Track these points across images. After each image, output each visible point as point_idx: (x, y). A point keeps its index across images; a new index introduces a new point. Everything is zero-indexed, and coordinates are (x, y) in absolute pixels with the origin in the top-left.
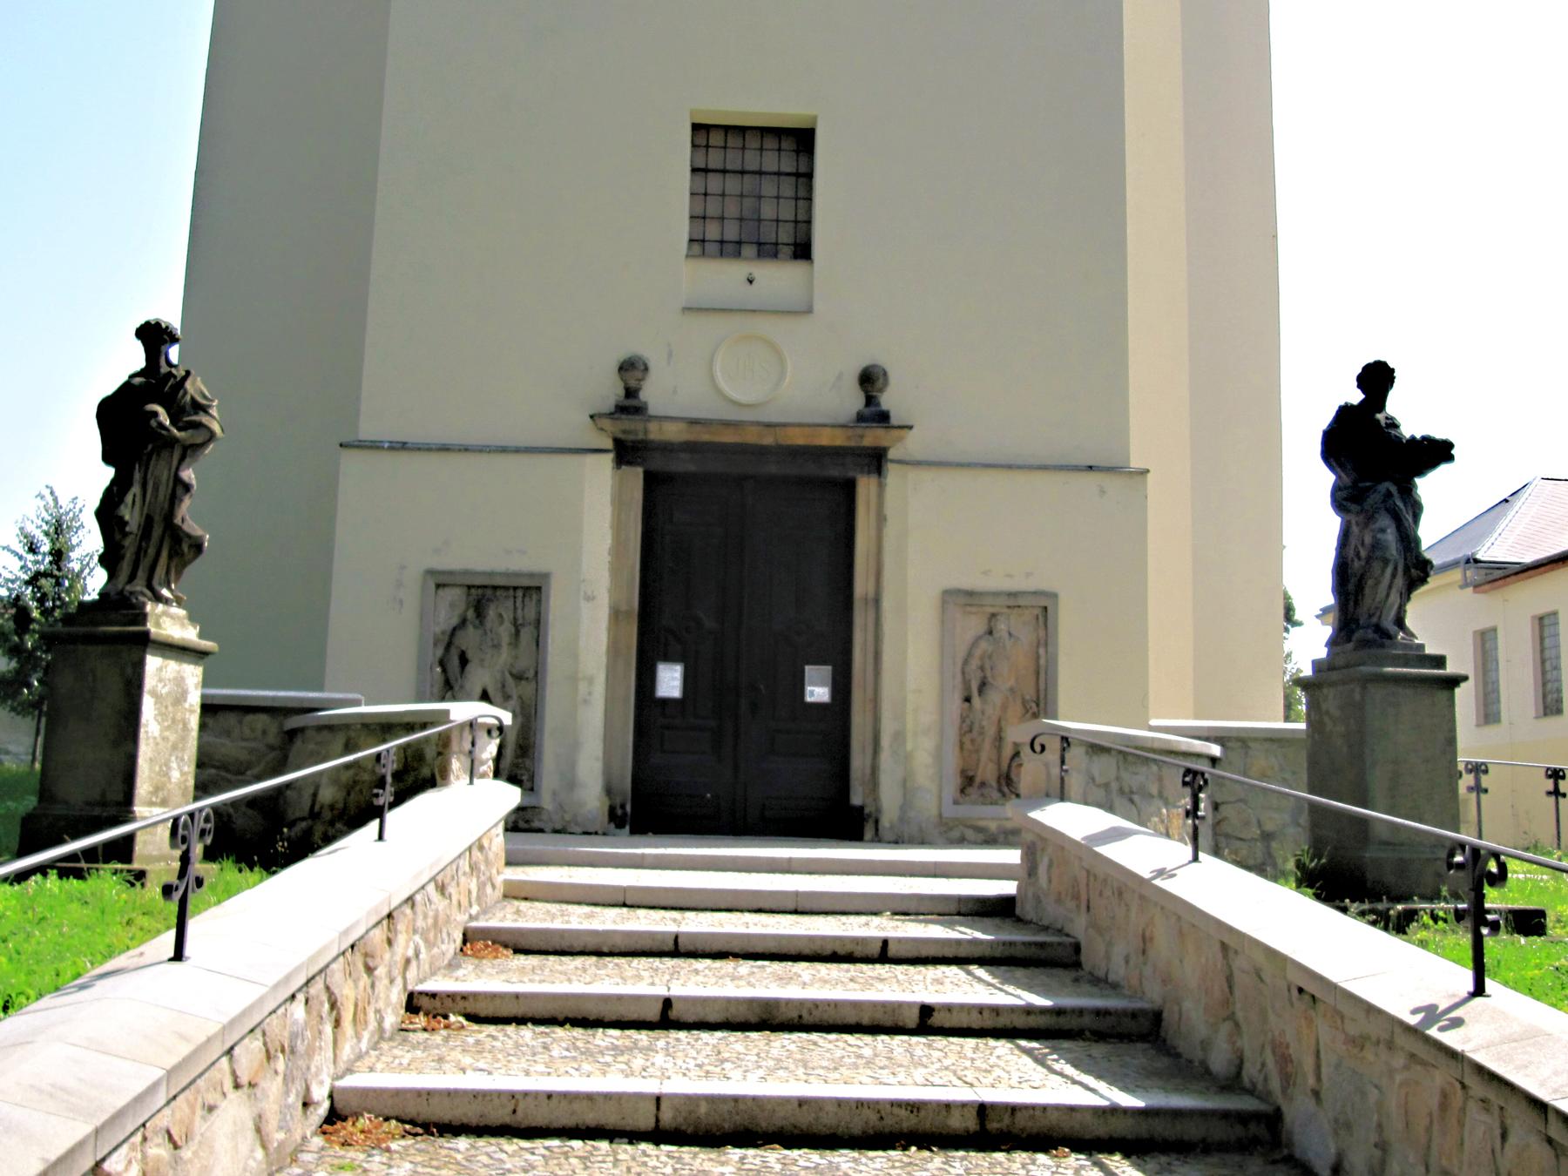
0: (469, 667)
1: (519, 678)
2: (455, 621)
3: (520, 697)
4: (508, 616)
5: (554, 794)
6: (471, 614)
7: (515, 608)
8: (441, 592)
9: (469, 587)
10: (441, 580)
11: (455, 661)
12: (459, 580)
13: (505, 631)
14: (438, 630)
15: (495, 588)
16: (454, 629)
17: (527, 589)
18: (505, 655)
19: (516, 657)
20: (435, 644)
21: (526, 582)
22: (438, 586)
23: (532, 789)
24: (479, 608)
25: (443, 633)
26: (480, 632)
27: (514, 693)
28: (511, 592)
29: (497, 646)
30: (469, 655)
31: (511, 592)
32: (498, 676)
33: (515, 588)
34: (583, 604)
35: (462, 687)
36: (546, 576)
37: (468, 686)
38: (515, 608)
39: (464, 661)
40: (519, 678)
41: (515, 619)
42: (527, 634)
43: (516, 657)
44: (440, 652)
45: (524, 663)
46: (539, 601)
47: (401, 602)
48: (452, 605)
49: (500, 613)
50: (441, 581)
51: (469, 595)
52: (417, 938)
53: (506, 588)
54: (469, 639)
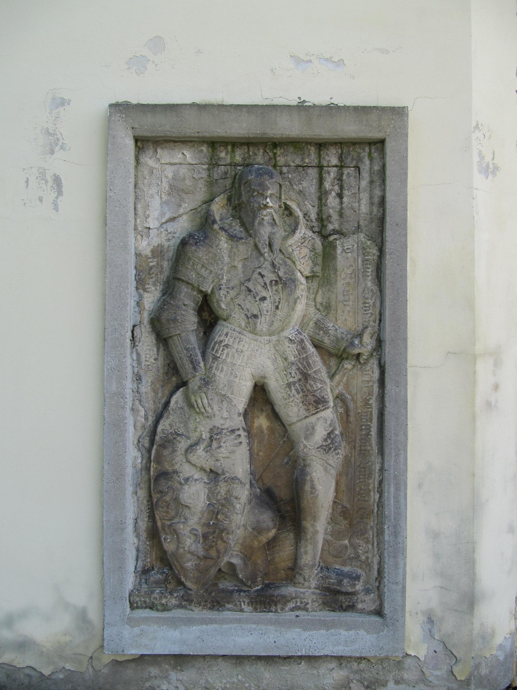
0: (221, 332)
1: (338, 355)
2: (183, 226)
3: (340, 398)
4: (305, 208)
5: (430, 620)
6: (218, 208)
7: (322, 195)
8: (149, 160)
9: (214, 144)
10: (150, 125)
11: (190, 320)
12: (192, 126)
13: (301, 248)
14: (145, 246)
15: (274, 144)
16: (184, 243)
17: (344, 145)
18: (302, 306)
19: (327, 308)
20: (141, 284)
21: (350, 129)
22: (141, 143)
23: (379, 613)
24: (243, 206)
25: (158, 252)
26: (244, 249)
27: (328, 389)
28: (312, 157)
29: (286, 283)
30: (223, 303)
31: (312, 157)
32: (291, 352)
33: (321, 145)
34: (478, 180)
35: (207, 382)
36: (399, 113)
37: (221, 377)
38: (322, 195)
39: (209, 317)
40: (338, 355)
41: (322, 220)
42: (349, 255)
43: (327, 308)
44: (151, 298)
45: (344, 321)
46: (158, 482)
47: (57, 181)
48: (176, 190)
49: (286, 194)
50: (149, 131)
51: (213, 164)
52: (222, 444)
53: (296, 144)
54: (223, 263)
